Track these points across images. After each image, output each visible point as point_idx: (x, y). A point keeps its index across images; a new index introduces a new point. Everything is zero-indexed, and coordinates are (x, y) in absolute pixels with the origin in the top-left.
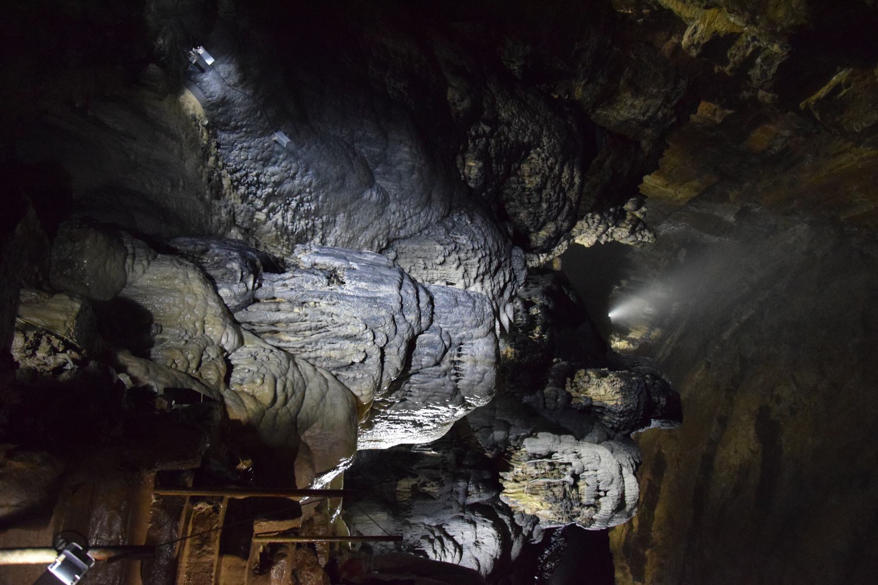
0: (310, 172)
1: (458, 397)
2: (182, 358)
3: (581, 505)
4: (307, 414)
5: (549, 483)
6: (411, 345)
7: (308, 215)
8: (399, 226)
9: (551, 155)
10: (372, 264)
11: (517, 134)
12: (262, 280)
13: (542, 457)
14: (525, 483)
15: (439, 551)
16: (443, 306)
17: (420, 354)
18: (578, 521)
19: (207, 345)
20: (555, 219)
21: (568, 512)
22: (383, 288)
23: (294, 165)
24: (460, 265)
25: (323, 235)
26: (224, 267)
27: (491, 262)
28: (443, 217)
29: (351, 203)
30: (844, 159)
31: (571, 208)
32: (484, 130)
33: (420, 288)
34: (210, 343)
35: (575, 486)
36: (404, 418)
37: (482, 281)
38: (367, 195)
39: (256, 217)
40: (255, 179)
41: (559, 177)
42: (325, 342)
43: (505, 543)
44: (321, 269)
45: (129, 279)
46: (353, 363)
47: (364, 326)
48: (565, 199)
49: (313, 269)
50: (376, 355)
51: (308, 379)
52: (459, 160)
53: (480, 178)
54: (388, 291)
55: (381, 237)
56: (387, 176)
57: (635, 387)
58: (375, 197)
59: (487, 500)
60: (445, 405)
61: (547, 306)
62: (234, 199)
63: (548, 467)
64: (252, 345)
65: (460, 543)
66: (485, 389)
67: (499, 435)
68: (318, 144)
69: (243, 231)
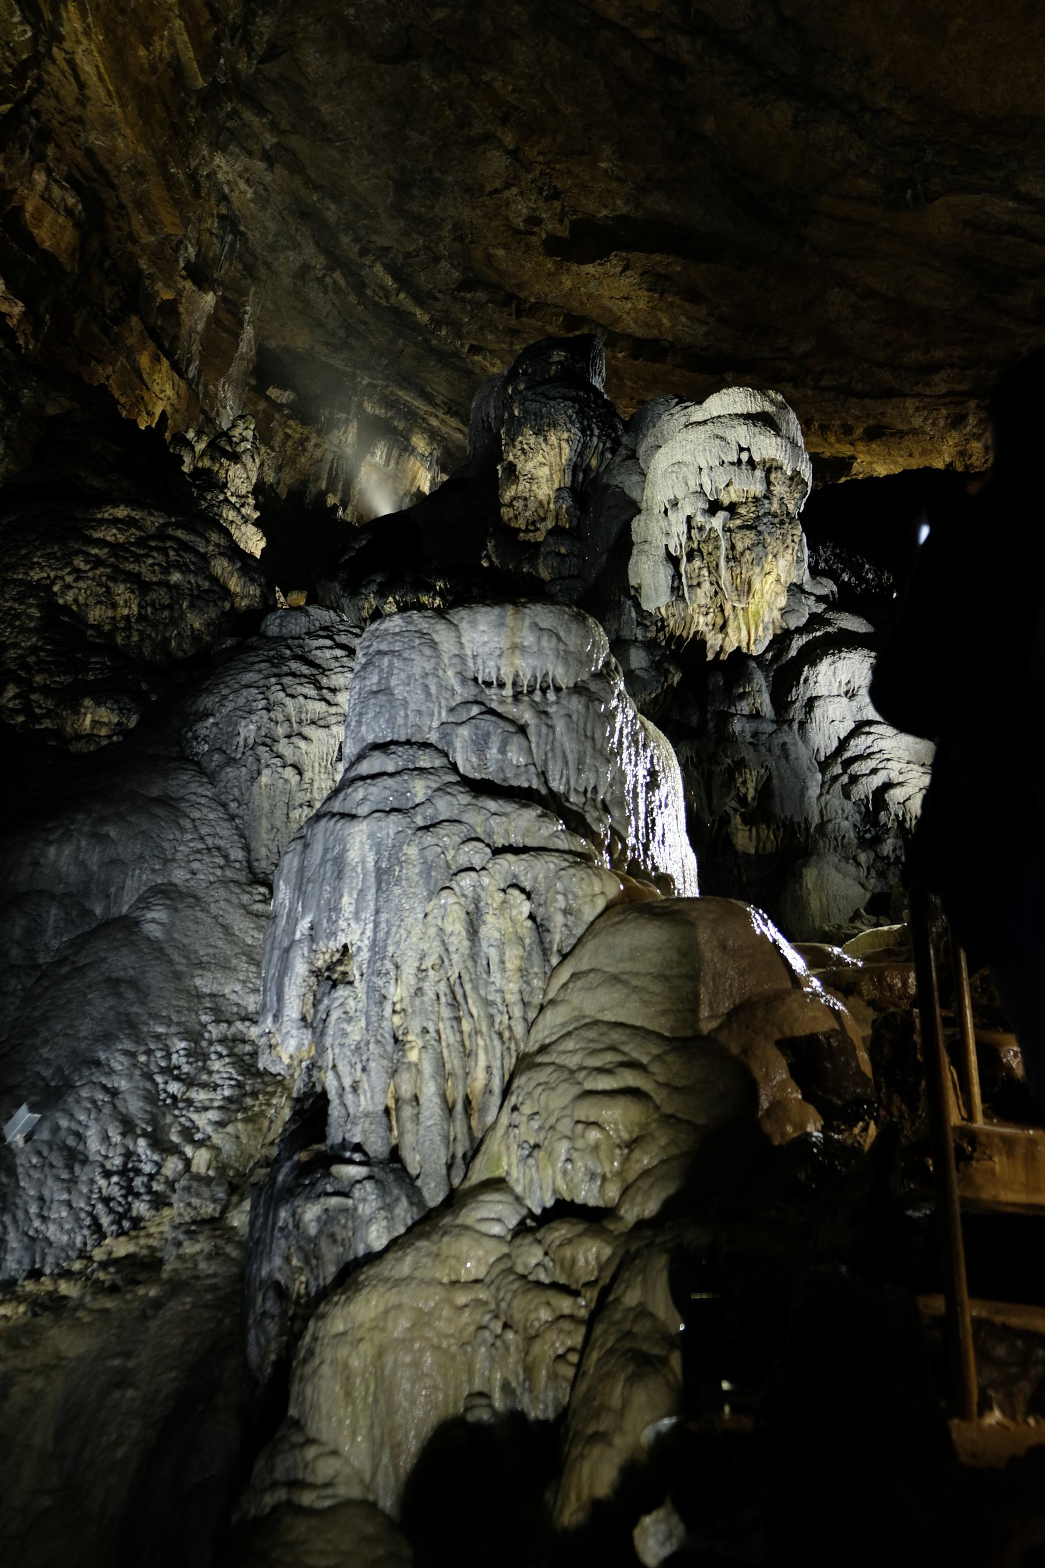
0: (102, 1056)
1: (593, 687)
2: (552, 1336)
3: (768, 496)
4: (663, 1013)
6: (482, 788)
7: (197, 1055)
8: (222, 862)
9: (70, 564)
10: (300, 888)
11: (23, 630)
12: (344, 1145)
13: (677, 575)
14: (728, 608)
15: (871, 764)
16: (391, 721)
17: (502, 770)
18: (796, 505)
19: (511, 1270)
20: (205, 558)
21: (782, 523)
22: (353, 856)
23: (85, 1093)
24: (300, 735)
25: (243, 1020)
26: (315, 1240)
27: (293, 675)
28: (202, 771)
29: (170, 962)
30: (87, 68)
31: (178, 525)
32: (15, 697)
33: (352, 774)
34: (506, 1264)
35: (732, 509)
36: (642, 808)
37: (334, 691)
38: (155, 931)
39: (203, 1171)
40: (115, 1179)
42: (487, 983)
44: (314, 1005)
45: (355, 1492)
46: (532, 917)
47: (445, 893)
48: (161, 535)
49: (314, 1024)
50: (509, 863)
51: (576, 1019)
52: (81, 746)
53: (117, 702)
54: (359, 843)
55: (245, 898)
56: (113, 890)
57: (533, 406)
58: (158, 914)
59: (766, 678)
60: (611, 715)
61: (380, 585)
62: (161, 1226)
63: (697, 563)
64: (503, 1158)
65: (853, 725)
66: (574, 626)
69: (235, 1199)
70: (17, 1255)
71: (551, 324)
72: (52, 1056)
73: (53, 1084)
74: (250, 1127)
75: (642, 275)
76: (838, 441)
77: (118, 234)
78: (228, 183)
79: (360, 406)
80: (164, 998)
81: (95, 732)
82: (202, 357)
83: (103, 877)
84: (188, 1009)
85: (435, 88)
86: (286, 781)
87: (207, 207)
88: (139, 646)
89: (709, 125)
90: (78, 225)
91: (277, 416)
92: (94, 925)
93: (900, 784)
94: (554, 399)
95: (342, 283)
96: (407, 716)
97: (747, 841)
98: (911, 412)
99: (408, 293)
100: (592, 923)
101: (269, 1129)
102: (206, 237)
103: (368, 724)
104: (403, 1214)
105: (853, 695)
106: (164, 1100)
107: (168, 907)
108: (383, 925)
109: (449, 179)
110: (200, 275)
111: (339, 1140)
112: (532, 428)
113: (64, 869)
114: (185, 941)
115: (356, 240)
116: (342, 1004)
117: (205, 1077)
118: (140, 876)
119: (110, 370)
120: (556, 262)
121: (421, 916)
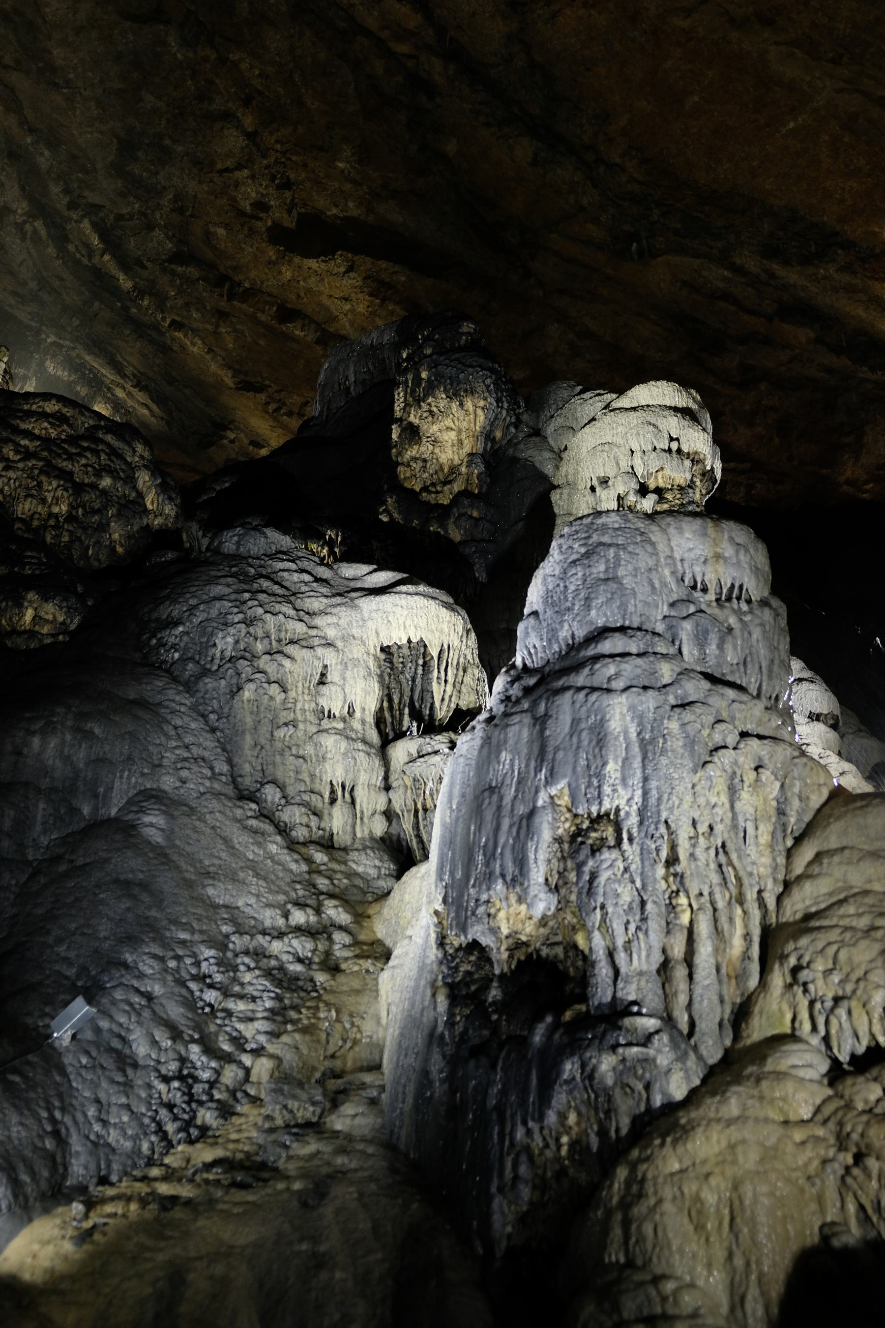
0: (129, 958)
7: (224, 964)
8: (209, 773)
16: (623, 607)
20: (132, 468)
22: (615, 725)
25: (264, 933)
28: (175, 680)
29: (178, 868)
35: (659, 491)
38: (158, 838)
41: (47, 441)
52: (21, 643)
55: (239, 812)
56: (101, 790)
68: (51, 940)
70: (83, 1159)
71: (263, 312)
72: (72, 954)
73: (80, 984)
74: (307, 1038)
79: (41, 364)
80: (181, 904)
81: (37, 628)
83: (90, 775)
84: (207, 918)
85: (179, 56)
86: (272, 698)
88: (69, 546)
89: (451, 147)
92: (82, 825)
95: (43, 233)
96: (636, 606)
99: (113, 255)
100: (819, 811)
101: (328, 1042)
103: (599, 609)
104: (694, 1067)
106: (203, 1009)
107: (164, 813)
108: (654, 792)
109: (180, 148)
111: (608, 998)
112: (446, 391)
113: (50, 762)
114: (188, 849)
115: (67, 191)
116: (611, 865)
117: (237, 988)
118: (129, 778)
120: (279, 250)
121: (690, 786)
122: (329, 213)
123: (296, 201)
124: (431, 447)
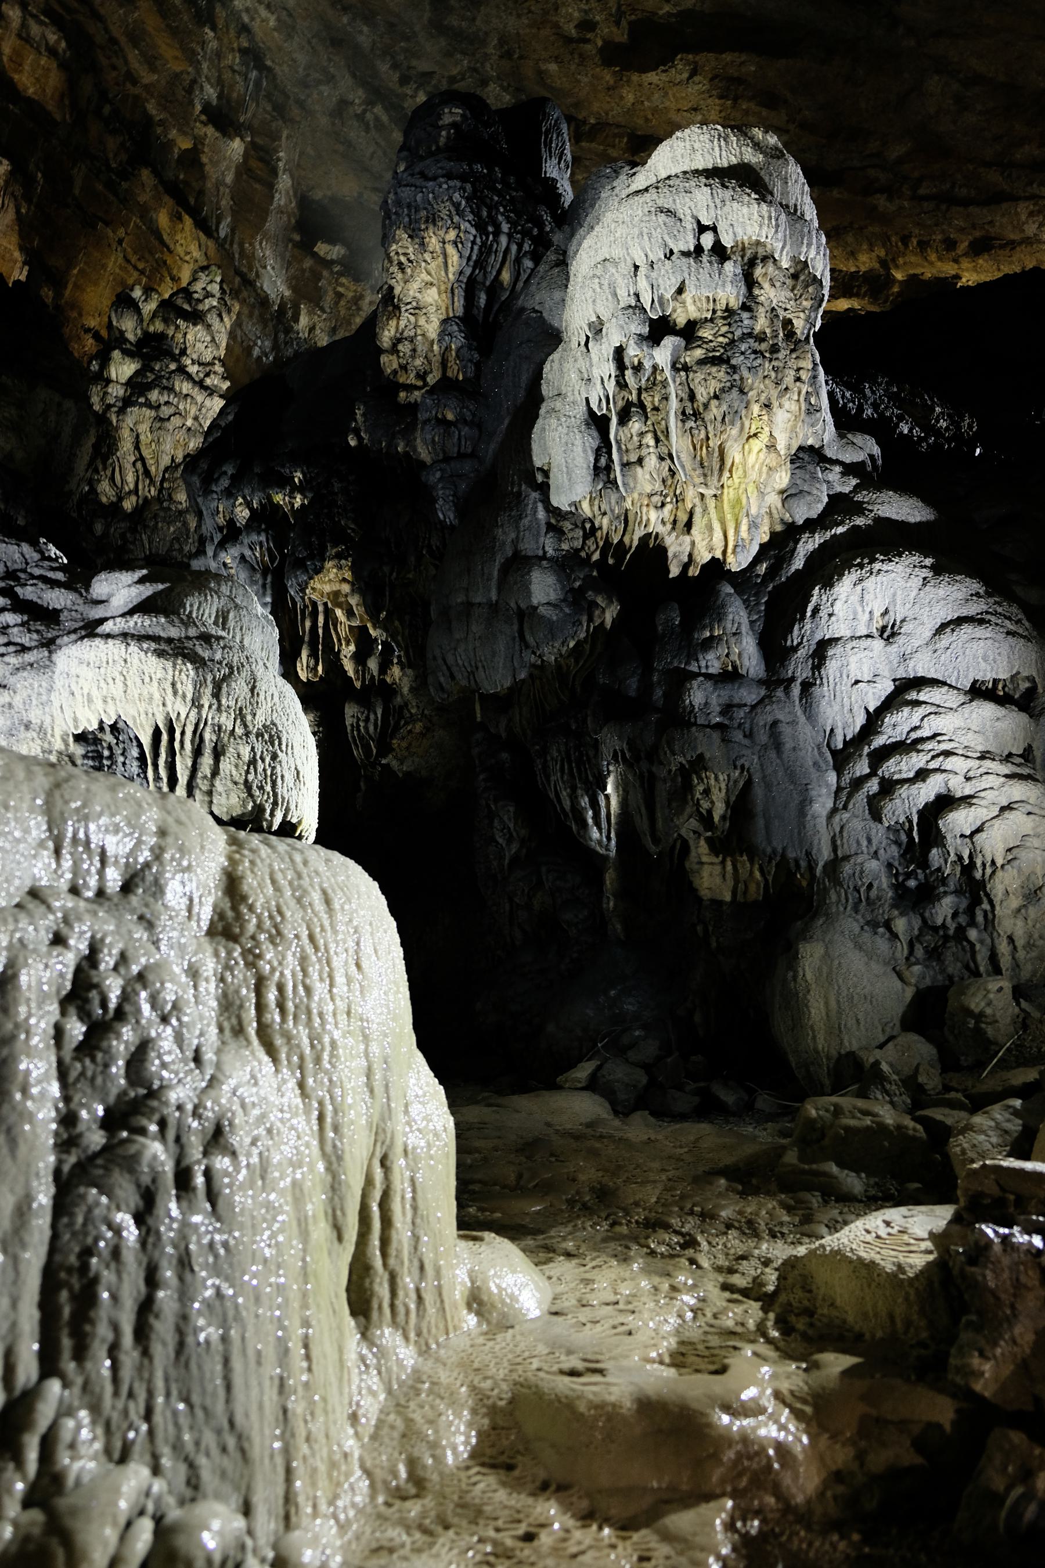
5: (684, 416)
13: (604, 446)
14: (691, 497)
21: (774, 349)
35: (689, 332)
43: (886, 541)
63: (635, 425)
65: (890, 687)
67: (543, 588)
71: (614, 146)
75: (712, 80)
76: (940, 259)
77: (114, 74)
78: (247, 10)
82: (235, 214)
87: (225, 41)
90: (63, 66)
91: (325, 273)
93: (967, 800)
94: (434, 178)
95: (385, 118)
97: (718, 880)
98: (1023, 218)
102: (227, 75)
105: (893, 634)
110: (223, 118)
115: (395, 66)
119: (121, 232)
120: (615, 72)
122: (661, 12)
123: (623, 8)
124: (412, 319)
